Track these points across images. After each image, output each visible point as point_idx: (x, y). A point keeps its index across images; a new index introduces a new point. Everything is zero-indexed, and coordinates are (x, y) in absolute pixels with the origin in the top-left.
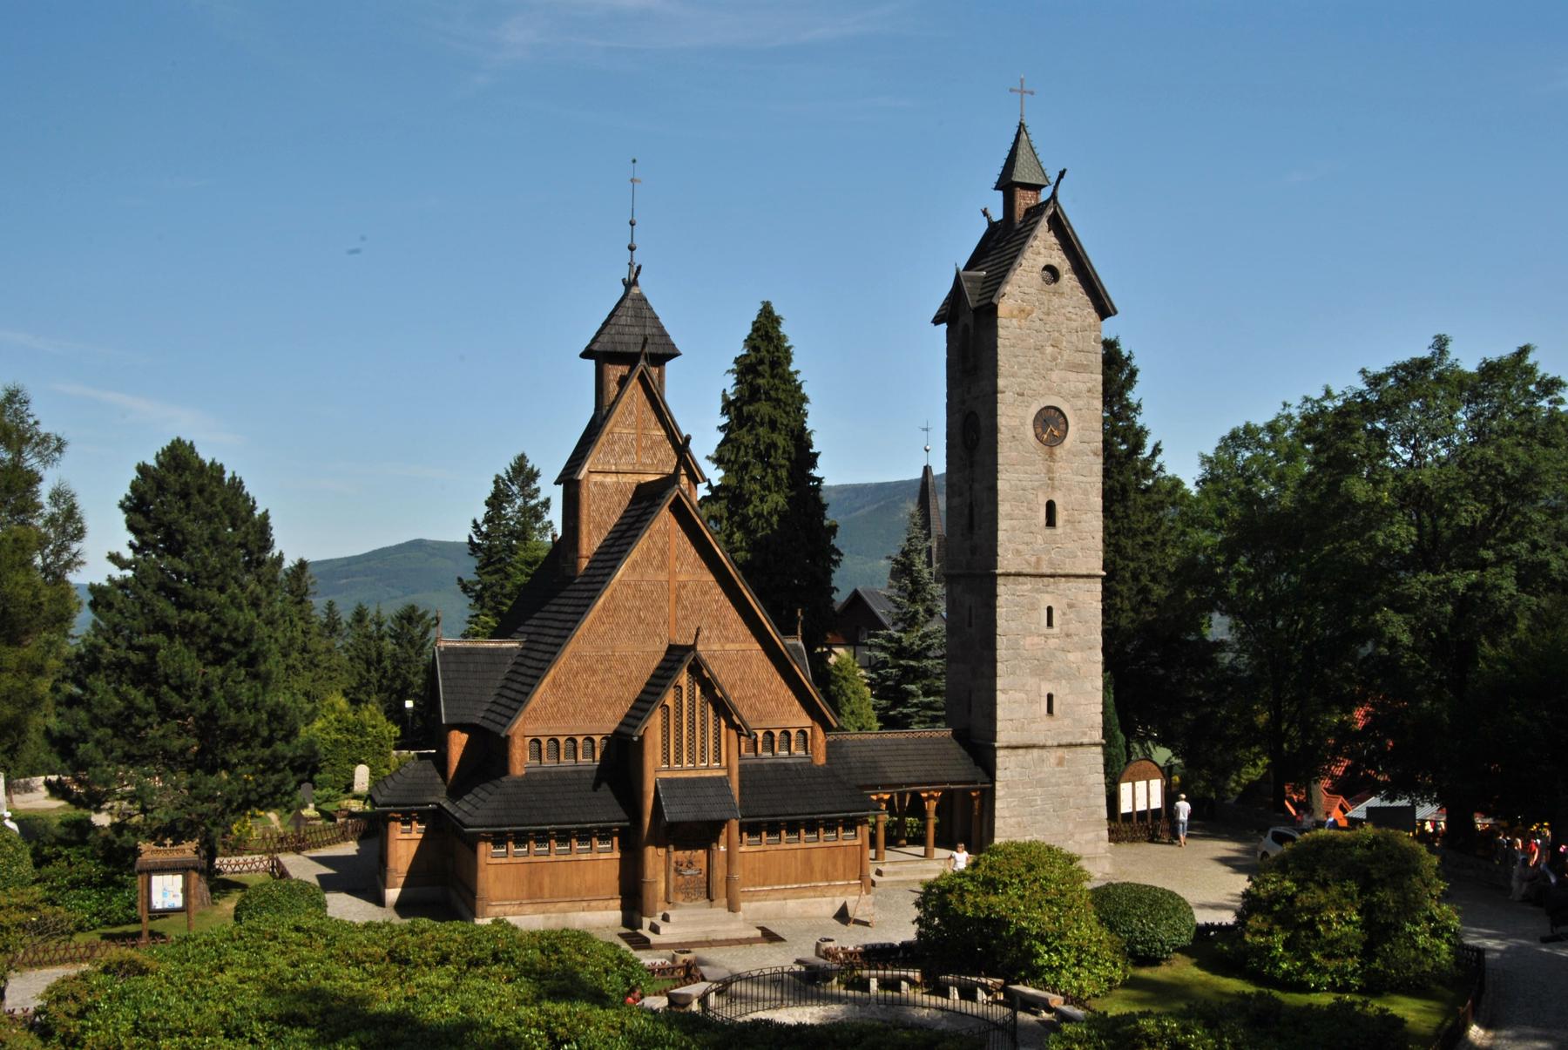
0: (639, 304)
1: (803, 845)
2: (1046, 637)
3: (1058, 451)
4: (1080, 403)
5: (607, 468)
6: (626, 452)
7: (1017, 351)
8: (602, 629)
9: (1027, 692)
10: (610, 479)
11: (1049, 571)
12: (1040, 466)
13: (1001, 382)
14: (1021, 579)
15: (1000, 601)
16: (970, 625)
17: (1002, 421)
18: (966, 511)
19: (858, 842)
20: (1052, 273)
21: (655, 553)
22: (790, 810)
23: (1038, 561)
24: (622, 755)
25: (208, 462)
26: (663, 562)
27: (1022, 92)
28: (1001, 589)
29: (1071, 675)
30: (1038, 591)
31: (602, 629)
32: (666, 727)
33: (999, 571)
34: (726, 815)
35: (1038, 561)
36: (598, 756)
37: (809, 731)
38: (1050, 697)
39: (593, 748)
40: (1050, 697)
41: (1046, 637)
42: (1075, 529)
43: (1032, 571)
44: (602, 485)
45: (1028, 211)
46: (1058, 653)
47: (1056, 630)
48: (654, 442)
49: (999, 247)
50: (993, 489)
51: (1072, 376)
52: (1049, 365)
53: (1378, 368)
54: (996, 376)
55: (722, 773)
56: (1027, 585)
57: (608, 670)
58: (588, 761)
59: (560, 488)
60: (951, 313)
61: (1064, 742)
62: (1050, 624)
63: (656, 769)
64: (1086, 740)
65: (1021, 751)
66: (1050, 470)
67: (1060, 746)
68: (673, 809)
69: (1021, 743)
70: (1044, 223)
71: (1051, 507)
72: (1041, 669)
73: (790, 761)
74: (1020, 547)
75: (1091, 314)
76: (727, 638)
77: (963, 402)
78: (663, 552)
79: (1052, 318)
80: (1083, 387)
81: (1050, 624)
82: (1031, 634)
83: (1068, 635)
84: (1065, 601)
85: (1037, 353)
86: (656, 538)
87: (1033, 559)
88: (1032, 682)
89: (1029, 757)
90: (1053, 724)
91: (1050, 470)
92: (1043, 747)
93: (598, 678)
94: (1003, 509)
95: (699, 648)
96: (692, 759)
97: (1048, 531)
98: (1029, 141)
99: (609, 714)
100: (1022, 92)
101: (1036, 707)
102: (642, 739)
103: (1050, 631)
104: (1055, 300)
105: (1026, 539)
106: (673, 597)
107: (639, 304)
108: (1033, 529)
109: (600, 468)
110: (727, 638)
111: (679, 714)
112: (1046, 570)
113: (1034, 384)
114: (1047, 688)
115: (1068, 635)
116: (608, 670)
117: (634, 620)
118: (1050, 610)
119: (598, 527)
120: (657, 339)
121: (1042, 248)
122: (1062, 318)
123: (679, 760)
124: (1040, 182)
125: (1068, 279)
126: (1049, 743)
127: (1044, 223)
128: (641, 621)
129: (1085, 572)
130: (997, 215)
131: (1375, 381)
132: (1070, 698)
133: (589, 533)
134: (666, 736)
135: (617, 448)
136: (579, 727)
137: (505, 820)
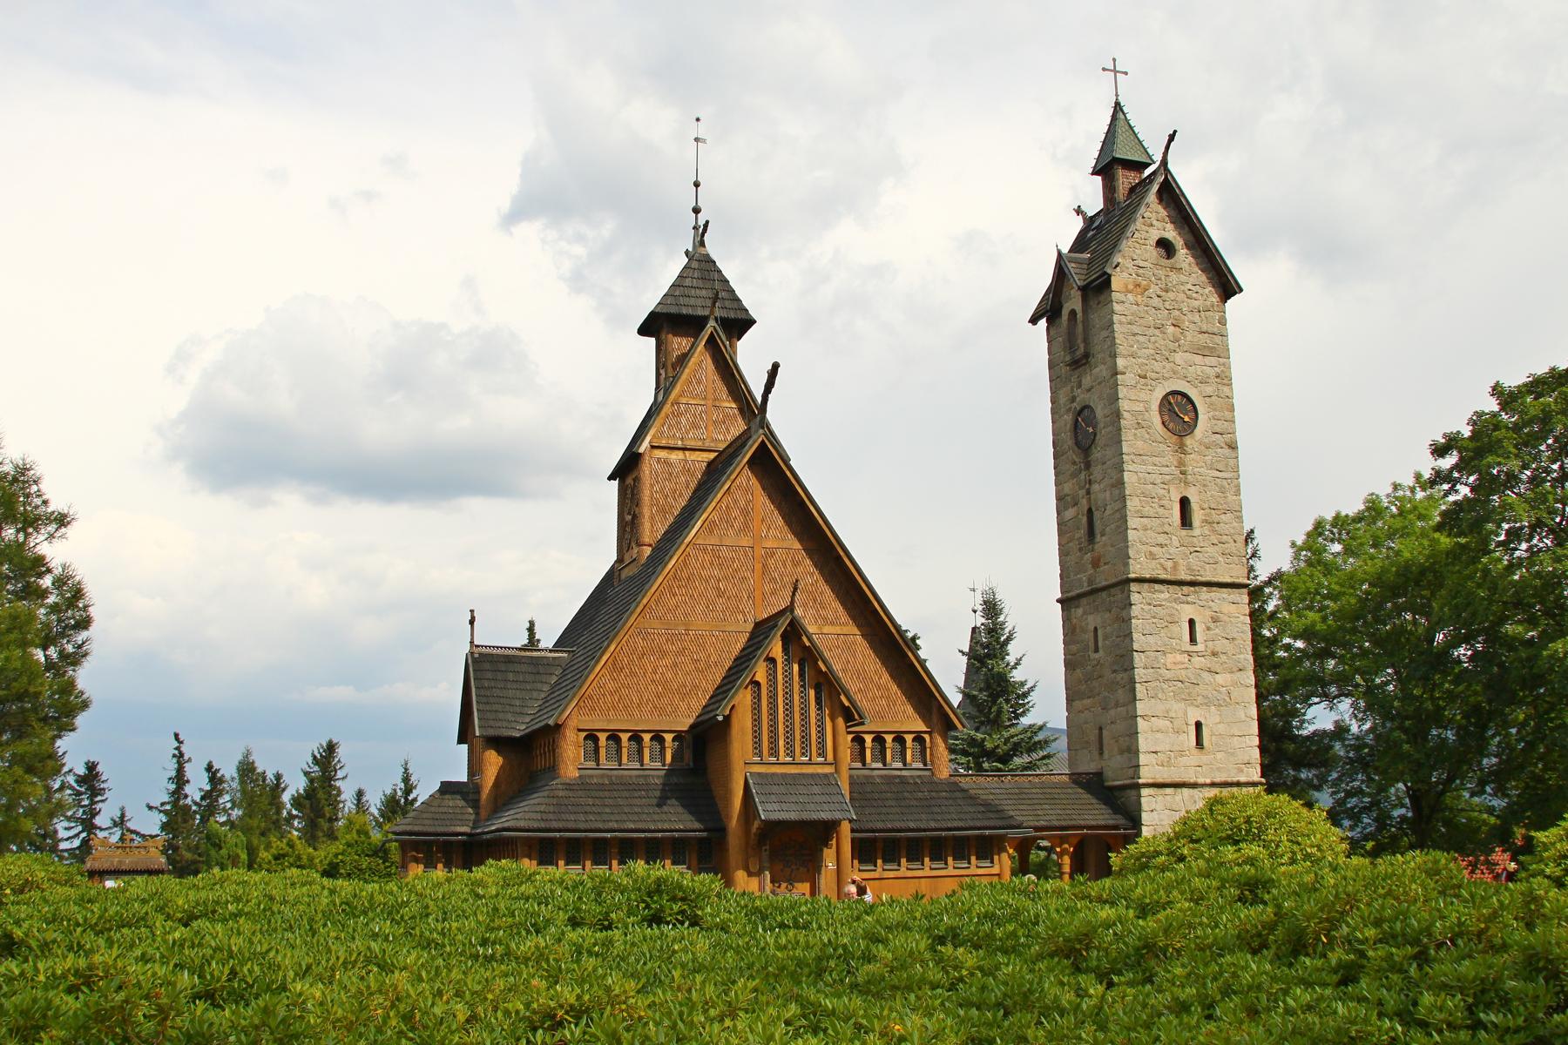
0: (708, 267)
1: (927, 872)
2: (1189, 654)
3: (1188, 441)
4: (1209, 390)
5: (672, 443)
6: (695, 426)
7: (1135, 329)
8: (673, 602)
9: (1171, 720)
10: (675, 456)
11: (1189, 578)
12: (1170, 458)
13: (1121, 363)
14: (1157, 586)
15: (1135, 611)
16: (1096, 650)
17: (1124, 405)
18: (1085, 519)
19: (996, 870)
20: (1165, 246)
21: (736, 513)
22: (912, 825)
23: (1175, 567)
24: (705, 740)
25: (259, 770)
26: (746, 525)
27: (1115, 71)
28: (1135, 598)
29: (1224, 701)
30: (1175, 600)
31: (673, 602)
32: (756, 707)
33: (1138, 568)
34: (838, 815)
35: (1175, 567)
36: (669, 759)
37: (927, 737)
38: (1198, 725)
39: (663, 749)
40: (1198, 725)
41: (1189, 654)
42: (1214, 531)
43: (1169, 577)
44: (666, 462)
45: (1132, 190)
46: (1205, 675)
47: (1200, 647)
48: (726, 416)
49: (1099, 236)
50: (1120, 483)
51: (1198, 359)
52: (1172, 346)
53: (1514, 379)
54: (1114, 356)
55: (829, 770)
56: (1164, 594)
57: (681, 652)
58: (655, 764)
59: (615, 483)
60: (1049, 310)
61: (1217, 780)
62: (1193, 640)
63: (743, 760)
64: (1243, 779)
65: (1169, 791)
66: (1181, 464)
67: (1213, 785)
68: (769, 807)
69: (1168, 780)
70: (1152, 196)
71: (1184, 503)
72: (1186, 689)
73: (904, 773)
74: (1155, 550)
75: (1211, 295)
76: (825, 619)
77: (1073, 399)
78: (745, 512)
79: (1171, 295)
80: (1211, 372)
81: (1193, 640)
82: (1174, 650)
83: (1214, 654)
84: (1208, 613)
85: (1157, 332)
86: (738, 495)
87: (1169, 564)
88: (1176, 707)
89: (1178, 798)
90: (1204, 758)
91: (1181, 464)
92: (1194, 786)
93: (667, 661)
94: (1132, 504)
95: (799, 612)
96: (790, 751)
97: (1184, 533)
98: (1127, 120)
99: (683, 705)
100: (1115, 71)
101: (1183, 737)
102: (727, 718)
103: (1194, 648)
104: (1174, 276)
105: (1162, 539)
106: (758, 566)
107: (708, 267)
108: (1167, 528)
109: (664, 443)
110: (825, 619)
111: (773, 697)
112: (1183, 575)
113: (1157, 366)
114: (1194, 715)
115: (1214, 654)
116: (681, 652)
117: (711, 593)
118: (1192, 622)
119: (663, 511)
120: (727, 304)
121: (1153, 222)
122: (1182, 296)
123: (774, 751)
124: (1144, 159)
125: (1183, 256)
126: (1201, 781)
127: (1152, 196)
128: (720, 594)
129: (1229, 580)
130: (1095, 204)
131: (1507, 398)
132: (1221, 728)
133: (652, 518)
134: (757, 721)
135: (683, 421)
136: (646, 722)
137: (555, 825)
